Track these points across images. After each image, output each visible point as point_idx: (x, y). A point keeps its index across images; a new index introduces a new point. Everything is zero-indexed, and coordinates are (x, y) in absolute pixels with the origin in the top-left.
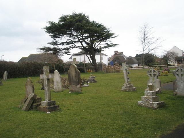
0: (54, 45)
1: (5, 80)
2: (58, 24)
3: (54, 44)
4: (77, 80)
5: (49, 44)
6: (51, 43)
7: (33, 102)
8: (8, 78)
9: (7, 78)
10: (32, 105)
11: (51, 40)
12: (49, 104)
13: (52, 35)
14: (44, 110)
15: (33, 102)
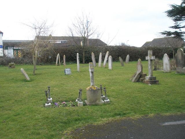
0: (175, 29)
1: (127, 62)
2: (181, 7)
3: (176, 27)
4: (183, 63)
5: (170, 27)
6: (172, 27)
7: (140, 77)
8: (130, 60)
9: (129, 61)
10: (139, 79)
11: (173, 24)
12: (151, 79)
13: (174, 18)
14: (147, 83)
15: (140, 77)
